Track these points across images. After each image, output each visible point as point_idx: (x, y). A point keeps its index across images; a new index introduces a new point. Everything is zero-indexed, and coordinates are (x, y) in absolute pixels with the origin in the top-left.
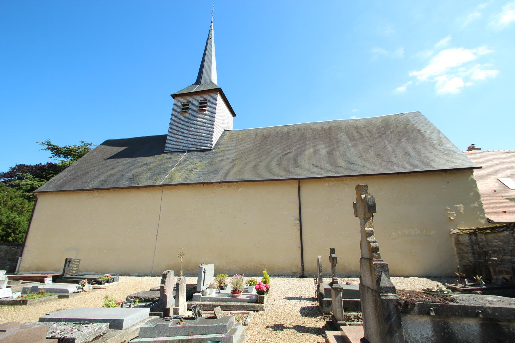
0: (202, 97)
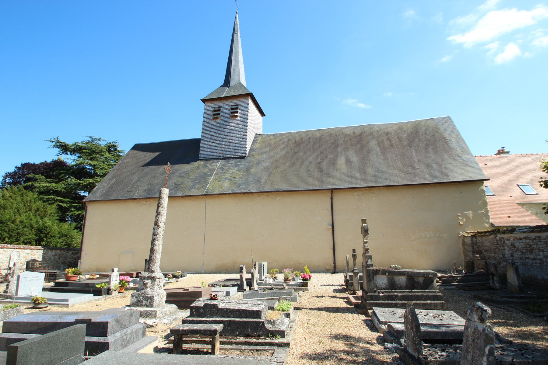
0: (233, 102)
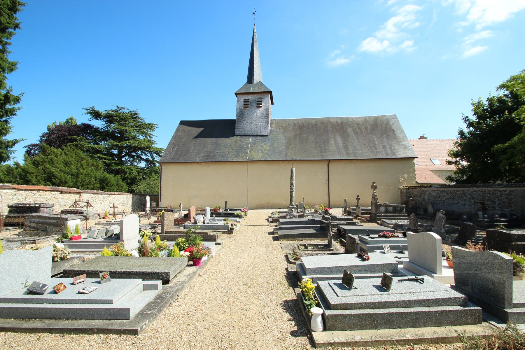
0: (259, 96)
